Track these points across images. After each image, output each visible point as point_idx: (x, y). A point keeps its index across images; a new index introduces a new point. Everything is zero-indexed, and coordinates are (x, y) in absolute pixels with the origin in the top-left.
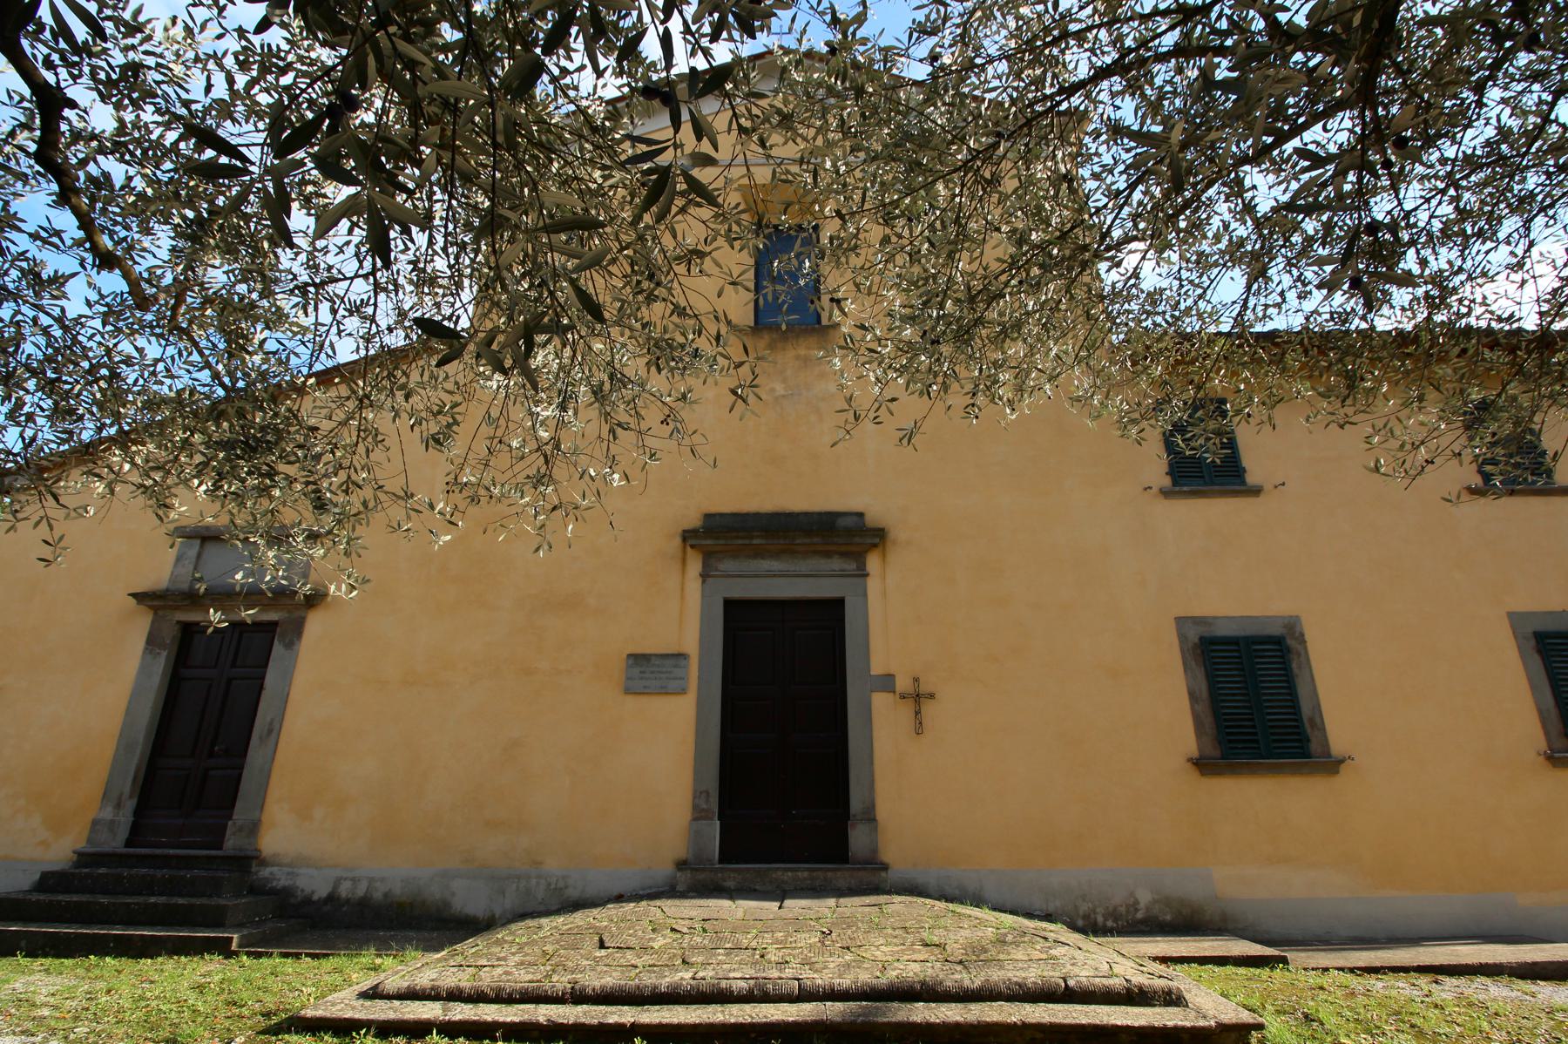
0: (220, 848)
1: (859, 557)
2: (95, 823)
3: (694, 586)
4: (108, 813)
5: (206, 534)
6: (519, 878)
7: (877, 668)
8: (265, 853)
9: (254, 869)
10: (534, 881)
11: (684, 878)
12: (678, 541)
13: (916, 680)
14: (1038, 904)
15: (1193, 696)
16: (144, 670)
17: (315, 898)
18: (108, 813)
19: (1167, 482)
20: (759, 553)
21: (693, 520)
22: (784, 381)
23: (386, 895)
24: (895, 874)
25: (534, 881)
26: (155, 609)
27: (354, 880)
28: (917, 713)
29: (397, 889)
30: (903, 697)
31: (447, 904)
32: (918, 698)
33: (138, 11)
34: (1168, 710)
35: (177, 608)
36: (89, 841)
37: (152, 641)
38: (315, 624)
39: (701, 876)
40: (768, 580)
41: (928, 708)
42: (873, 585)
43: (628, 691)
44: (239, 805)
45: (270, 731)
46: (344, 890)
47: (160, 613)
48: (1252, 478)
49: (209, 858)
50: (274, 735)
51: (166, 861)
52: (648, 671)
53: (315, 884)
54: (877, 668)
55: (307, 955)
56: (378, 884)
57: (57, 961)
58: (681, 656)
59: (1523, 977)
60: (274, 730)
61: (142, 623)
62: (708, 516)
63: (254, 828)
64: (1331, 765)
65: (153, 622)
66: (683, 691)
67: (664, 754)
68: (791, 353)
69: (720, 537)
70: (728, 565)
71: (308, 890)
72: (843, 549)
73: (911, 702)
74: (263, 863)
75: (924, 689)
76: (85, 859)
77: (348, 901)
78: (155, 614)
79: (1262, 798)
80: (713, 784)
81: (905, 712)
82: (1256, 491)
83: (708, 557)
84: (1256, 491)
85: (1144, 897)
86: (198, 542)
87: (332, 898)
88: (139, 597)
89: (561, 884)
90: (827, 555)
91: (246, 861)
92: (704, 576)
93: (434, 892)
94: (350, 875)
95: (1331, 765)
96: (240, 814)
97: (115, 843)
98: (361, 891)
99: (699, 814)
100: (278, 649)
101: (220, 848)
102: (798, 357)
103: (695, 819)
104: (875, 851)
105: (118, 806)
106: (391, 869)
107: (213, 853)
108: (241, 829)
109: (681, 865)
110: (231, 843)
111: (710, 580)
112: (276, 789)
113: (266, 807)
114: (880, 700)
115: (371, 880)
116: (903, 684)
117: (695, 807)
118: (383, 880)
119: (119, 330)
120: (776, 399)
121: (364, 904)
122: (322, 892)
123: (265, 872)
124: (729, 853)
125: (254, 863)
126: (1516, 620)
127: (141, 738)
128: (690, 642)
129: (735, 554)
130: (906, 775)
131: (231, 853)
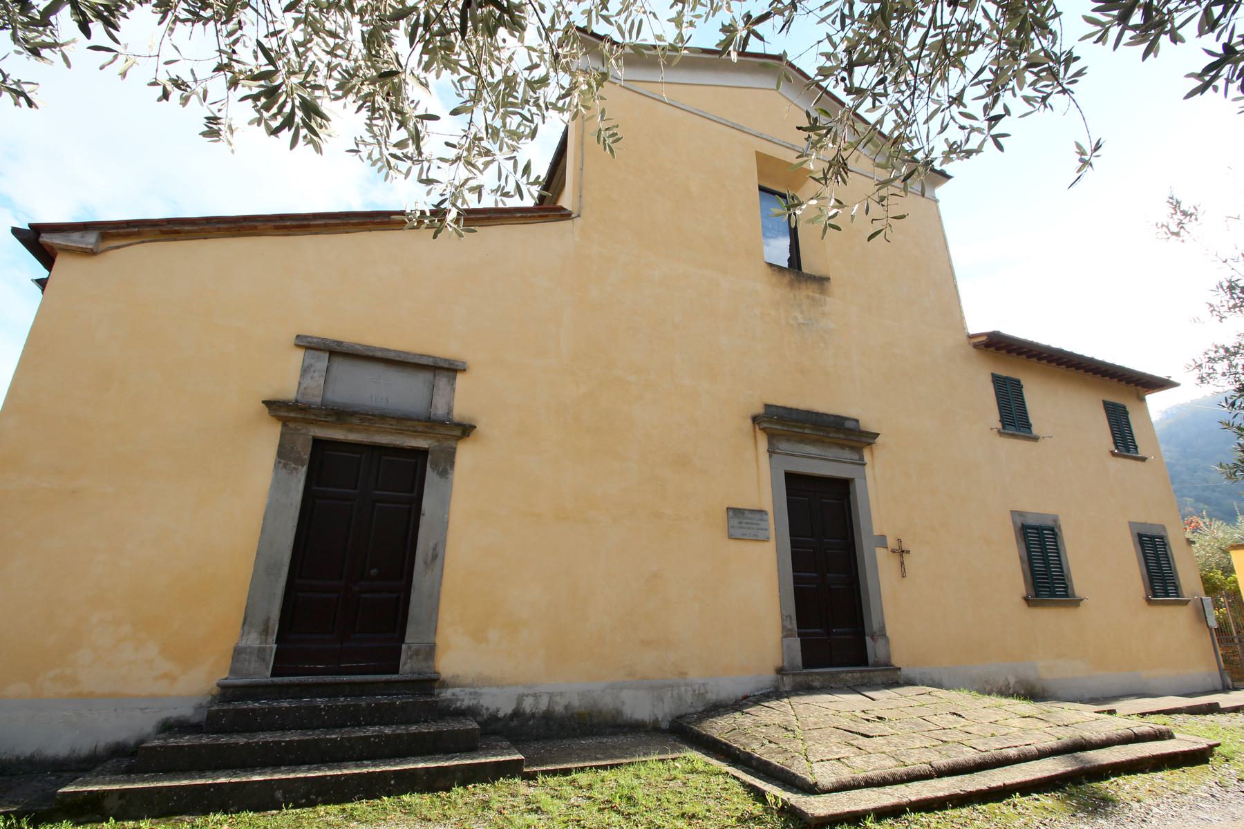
0: (397, 672)
1: (858, 450)
2: (238, 652)
3: (764, 458)
4: (253, 640)
5: (338, 349)
6: (672, 686)
7: (876, 532)
8: (896, 661)
9: (436, 691)
10: (683, 689)
11: (788, 682)
12: (749, 422)
13: (900, 541)
14: (1210, 688)
15: (1021, 558)
16: (277, 484)
17: (501, 714)
18: (253, 640)
19: (1000, 426)
20: (803, 439)
21: (759, 409)
22: (802, 312)
23: (566, 708)
24: (906, 671)
25: (683, 689)
26: (285, 422)
27: (535, 695)
28: (902, 563)
29: (576, 703)
30: (893, 551)
31: (619, 712)
32: (902, 552)
33: (124, 15)
34: (1008, 567)
35: (311, 422)
36: (233, 671)
37: (284, 454)
38: (465, 454)
39: (799, 679)
40: (811, 461)
42: (868, 470)
43: (730, 537)
44: (410, 629)
45: (435, 557)
46: (528, 705)
47: (292, 425)
48: (1035, 430)
49: (387, 682)
50: (438, 561)
51: (334, 690)
52: (741, 521)
53: (500, 702)
54: (876, 532)
55: (545, 773)
56: (558, 699)
58: (761, 512)
59: (1205, 713)
60: (436, 556)
61: (269, 436)
62: (767, 406)
63: (430, 652)
64: (1076, 602)
65: (282, 435)
66: (767, 540)
67: (754, 588)
68: (804, 293)
69: (781, 424)
70: (784, 446)
71: (492, 708)
72: (852, 444)
73: (897, 556)
74: (444, 685)
75: (904, 548)
76: (228, 692)
77: (533, 715)
78: (284, 425)
79: (1049, 617)
80: (792, 610)
81: (895, 560)
82: (1036, 439)
83: (772, 437)
84: (1036, 439)
85: (1012, 681)
86: (327, 355)
87: (517, 714)
88: (269, 404)
89: (702, 691)
90: (842, 447)
91: (428, 684)
92: (771, 452)
93: (607, 702)
94: (531, 691)
95: (1076, 602)
96: (412, 638)
97: (263, 674)
98: (543, 705)
99: (786, 633)
100: (431, 475)
101: (397, 672)
102: (808, 297)
103: (785, 636)
104: (889, 657)
105: (265, 631)
106: (565, 683)
107: (394, 677)
108: (417, 653)
109: (780, 671)
110: (408, 666)
111: (774, 456)
113: (439, 631)
114: (881, 553)
115: (551, 695)
116: (891, 543)
117: (784, 628)
118: (561, 694)
120: (799, 324)
121: (548, 716)
122: (506, 709)
123: (447, 694)
124: (808, 662)
125: (437, 684)
128: (767, 505)
129: (789, 438)
130: (901, 604)
131: (410, 677)
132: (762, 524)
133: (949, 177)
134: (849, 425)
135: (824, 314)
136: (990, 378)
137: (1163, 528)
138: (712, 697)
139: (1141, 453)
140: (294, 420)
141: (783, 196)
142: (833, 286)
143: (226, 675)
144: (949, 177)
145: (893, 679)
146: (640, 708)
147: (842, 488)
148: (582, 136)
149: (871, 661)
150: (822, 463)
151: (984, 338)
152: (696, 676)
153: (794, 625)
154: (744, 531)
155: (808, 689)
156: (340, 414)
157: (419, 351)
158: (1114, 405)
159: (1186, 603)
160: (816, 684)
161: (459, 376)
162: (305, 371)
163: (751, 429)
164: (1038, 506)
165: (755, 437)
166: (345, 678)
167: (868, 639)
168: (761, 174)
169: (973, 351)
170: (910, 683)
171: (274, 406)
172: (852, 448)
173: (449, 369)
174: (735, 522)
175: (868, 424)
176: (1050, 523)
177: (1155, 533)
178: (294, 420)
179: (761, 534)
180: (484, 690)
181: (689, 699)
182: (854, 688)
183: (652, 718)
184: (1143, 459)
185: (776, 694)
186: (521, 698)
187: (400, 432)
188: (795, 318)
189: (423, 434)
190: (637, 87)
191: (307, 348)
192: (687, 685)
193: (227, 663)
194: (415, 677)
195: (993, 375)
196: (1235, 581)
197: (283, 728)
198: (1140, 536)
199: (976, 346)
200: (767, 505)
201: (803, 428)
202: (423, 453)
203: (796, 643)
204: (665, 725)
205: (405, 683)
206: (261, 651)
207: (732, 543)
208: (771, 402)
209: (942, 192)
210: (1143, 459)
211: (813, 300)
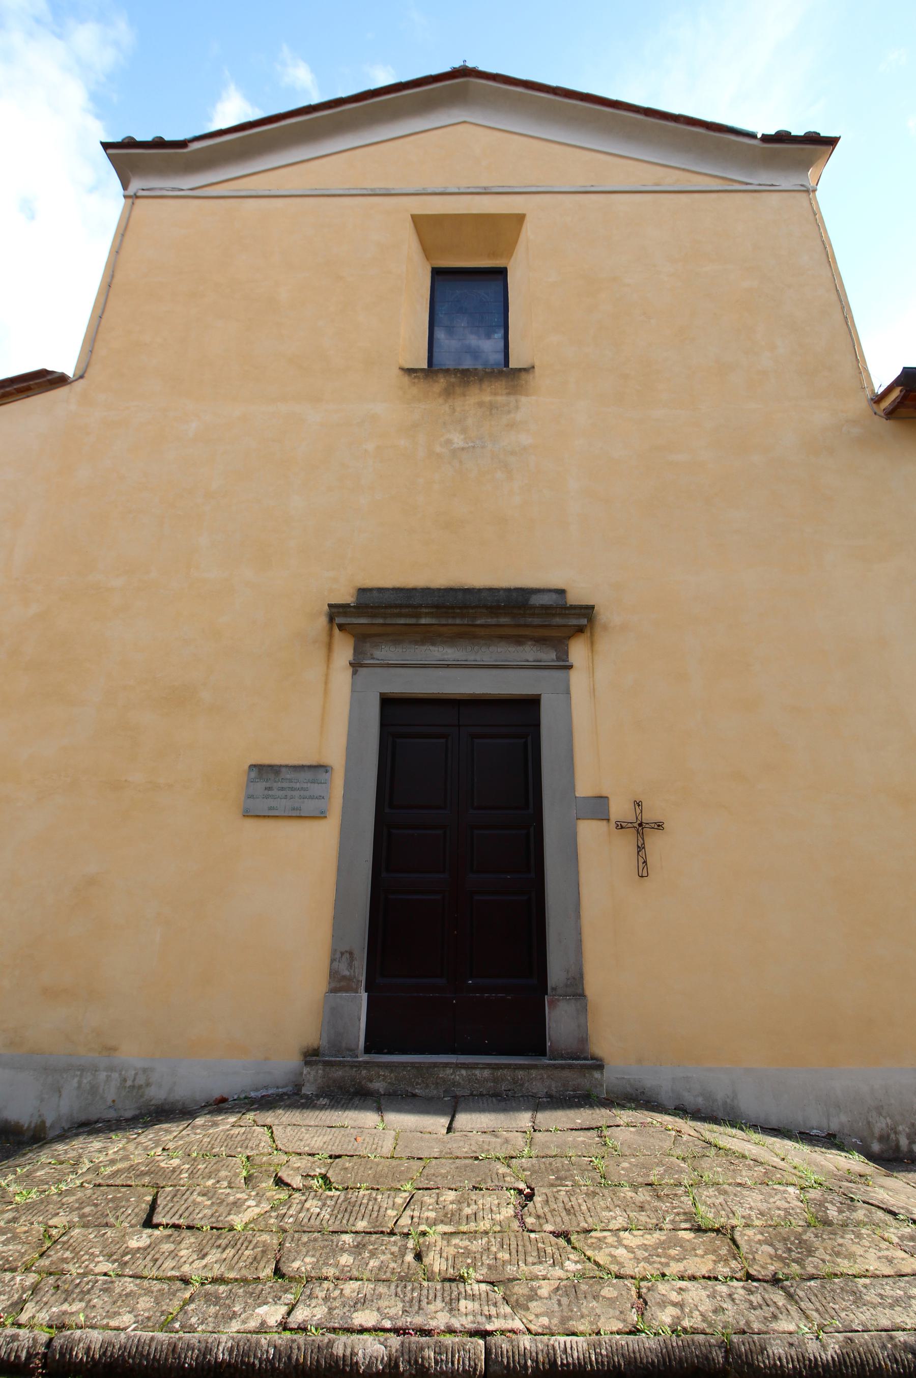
3: (342, 677)
6: (82, 1069)
7: (584, 788)
10: (103, 1076)
13: (638, 804)
20: (428, 637)
21: (346, 596)
22: (464, 431)
25: (103, 1076)
28: (640, 848)
30: (620, 826)
32: (641, 828)
42: (578, 680)
52: (275, 787)
54: (584, 788)
58: (323, 768)
62: (362, 591)
66: (321, 816)
67: (289, 907)
70: (386, 653)
75: (647, 817)
80: (358, 939)
81: (625, 844)
83: (363, 640)
89: (141, 1080)
90: (519, 641)
92: (356, 665)
99: (339, 984)
102: (481, 404)
104: (584, 1040)
109: (311, 1056)
111: (363, 671)
114: (589, 832)
116: (620, 809)
117: (334, 974)
120: (454, 453)
128: (334, 753)
132: (316, 789)
133: (832, 142)
135: (511, 426)
138: (157, 1094)
144: (832, 142)
145: (580, 1083)
147: (519, 721)
148: (113, 276)
151: (896, 393)
152: (132, 1054)
154: (271, 802)
160: (379, 1086)
163: (324, 637)
165: (330, 647)
168: (427, 251)
172: (541, 641)
174: (260, 786)
179: (309, 806)
181: (111, 1093)
182: (501, 1099)
183: (35, 1120)
185: (290, 1097)
188: (449, 442)
192: (111, 1069)
199: (890, 414)
201: (418, 616)
203: (359, 1004)
211: (492, 407)
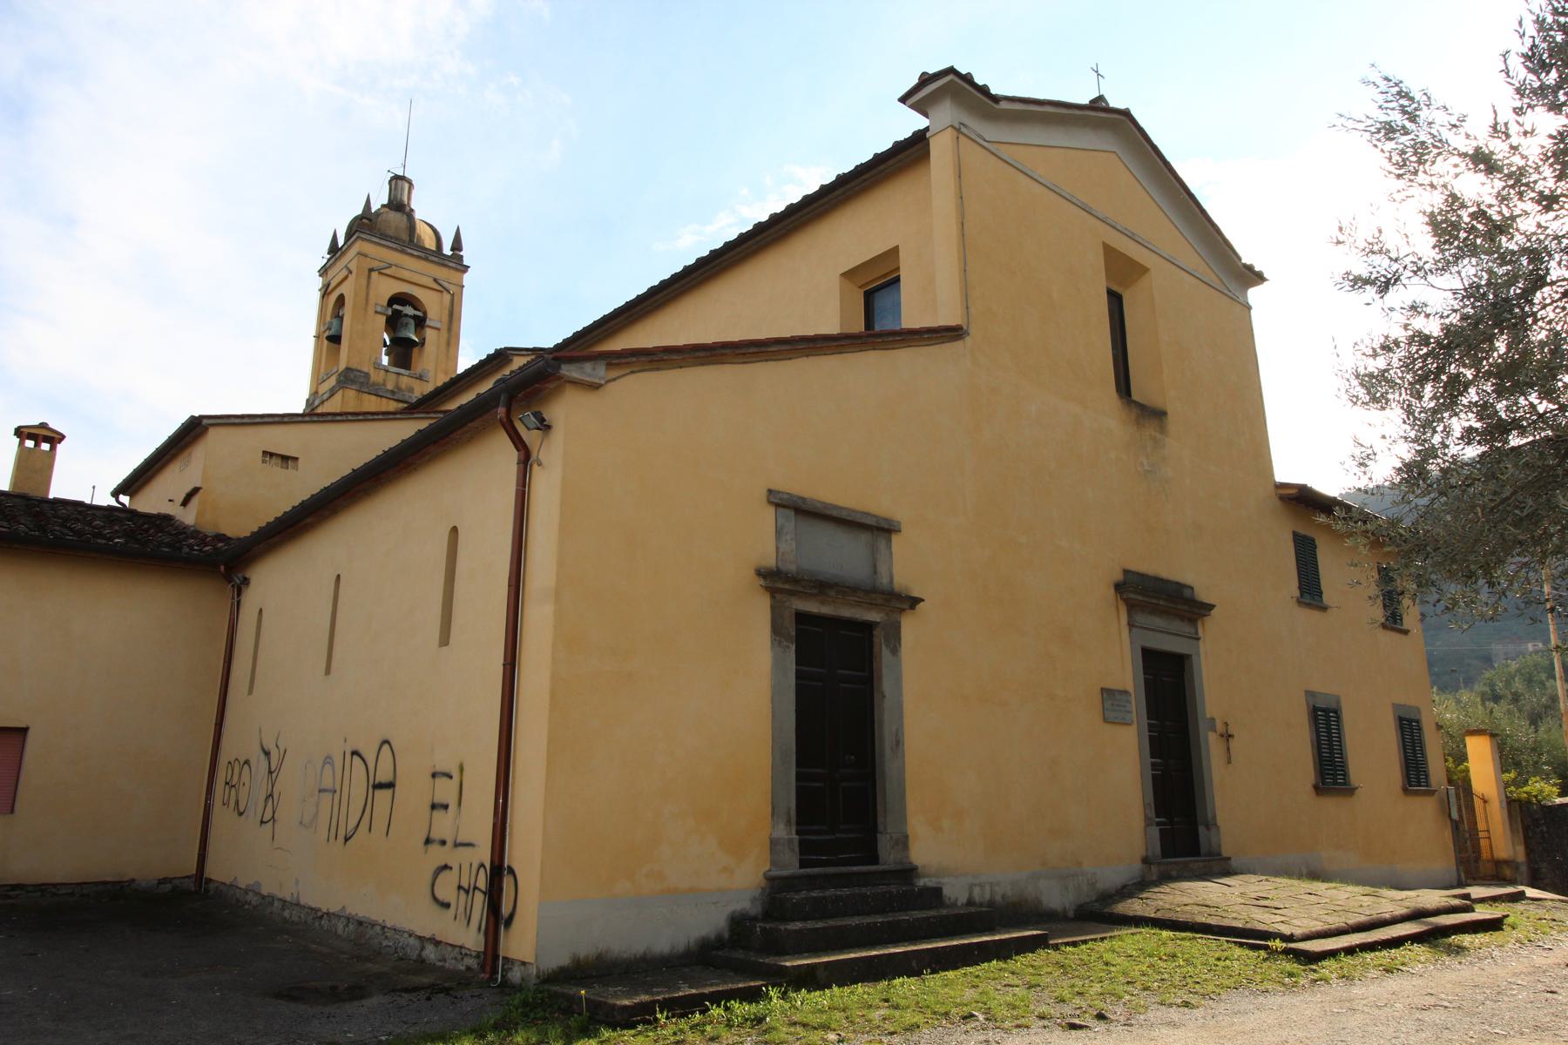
13: (1226, 724)
16: (777, 664)
19: (1297, 593)
23: (1003, 897)
32: (1227, 736)
35: (791, 593)
36: (774, 863)
38: (910, 627)
41: (1233, 743)
43: (1105, 720)
47: (778, 596)
57: (847, 990)
58: (1126, 692)
60: (898, 743)
61: (759, 612)
62: (1126, 572)
63: (903, 842)
65: (773, 608)
70: (1141, 619)
78: (773, 597)
83: (1132, 607)
84: (1324, 609)
92: (1131, 625)
97: (791, 865)
99: (1148, 822)
109: (1145, 861)
110: (888, 857)
112: (912, 804)
116: (1220, 727)
119: (527, 1016)
126: (1396, 707)
127: (885, 671)
128: (1130, 688)
129: (1155, 610)
131: (892, 867)
134: (1187, 593)
136: (1290, 537)
137: (1419, 710)
139: (1405, 626)
140: (781, 591)
141: (1115, 299)
142: (1171, 418)
143: (767, 868)
146: (1055, 897)
149: (1203, 849)
150: (838, 555)
153: (1152, 814)
155: (1166, 878)
156: (822, 587)
157: (859, 507)
158: (1305, 537)
159: (1431, 793)
161: (894, 538)
162: (779, 532)
164: (1325, 686)
166: (855, 869)
167: (1201, 829)
169: (1278, 503)
170: (1236, 874)
171: (763, 573)
173: (883, 530)
175: (1203, 595)
176: (1334, 706)
177: (1412, 716)
178: (781, 591)
180: (945, 880)
184: (1406, 632)
186: (971, 887)
187: (859, 604)
189: (873, 606)
190: (1004, 151)
191: (777, 505)
193: (767, 855)
194: (899, 867)
195: (1295, 534)
196: (1467, 771)
197: (845, 915)
198: (1401, 719)
199: (1282, 498)
200: (1130, 688)
202: (869, 627)
204: (1071, 914)
205: (883, 873)
206: (790, 840)
207: (1108, 727)
208: (1134, 567)
209: (1254, 295)
210: (1406, 632)
